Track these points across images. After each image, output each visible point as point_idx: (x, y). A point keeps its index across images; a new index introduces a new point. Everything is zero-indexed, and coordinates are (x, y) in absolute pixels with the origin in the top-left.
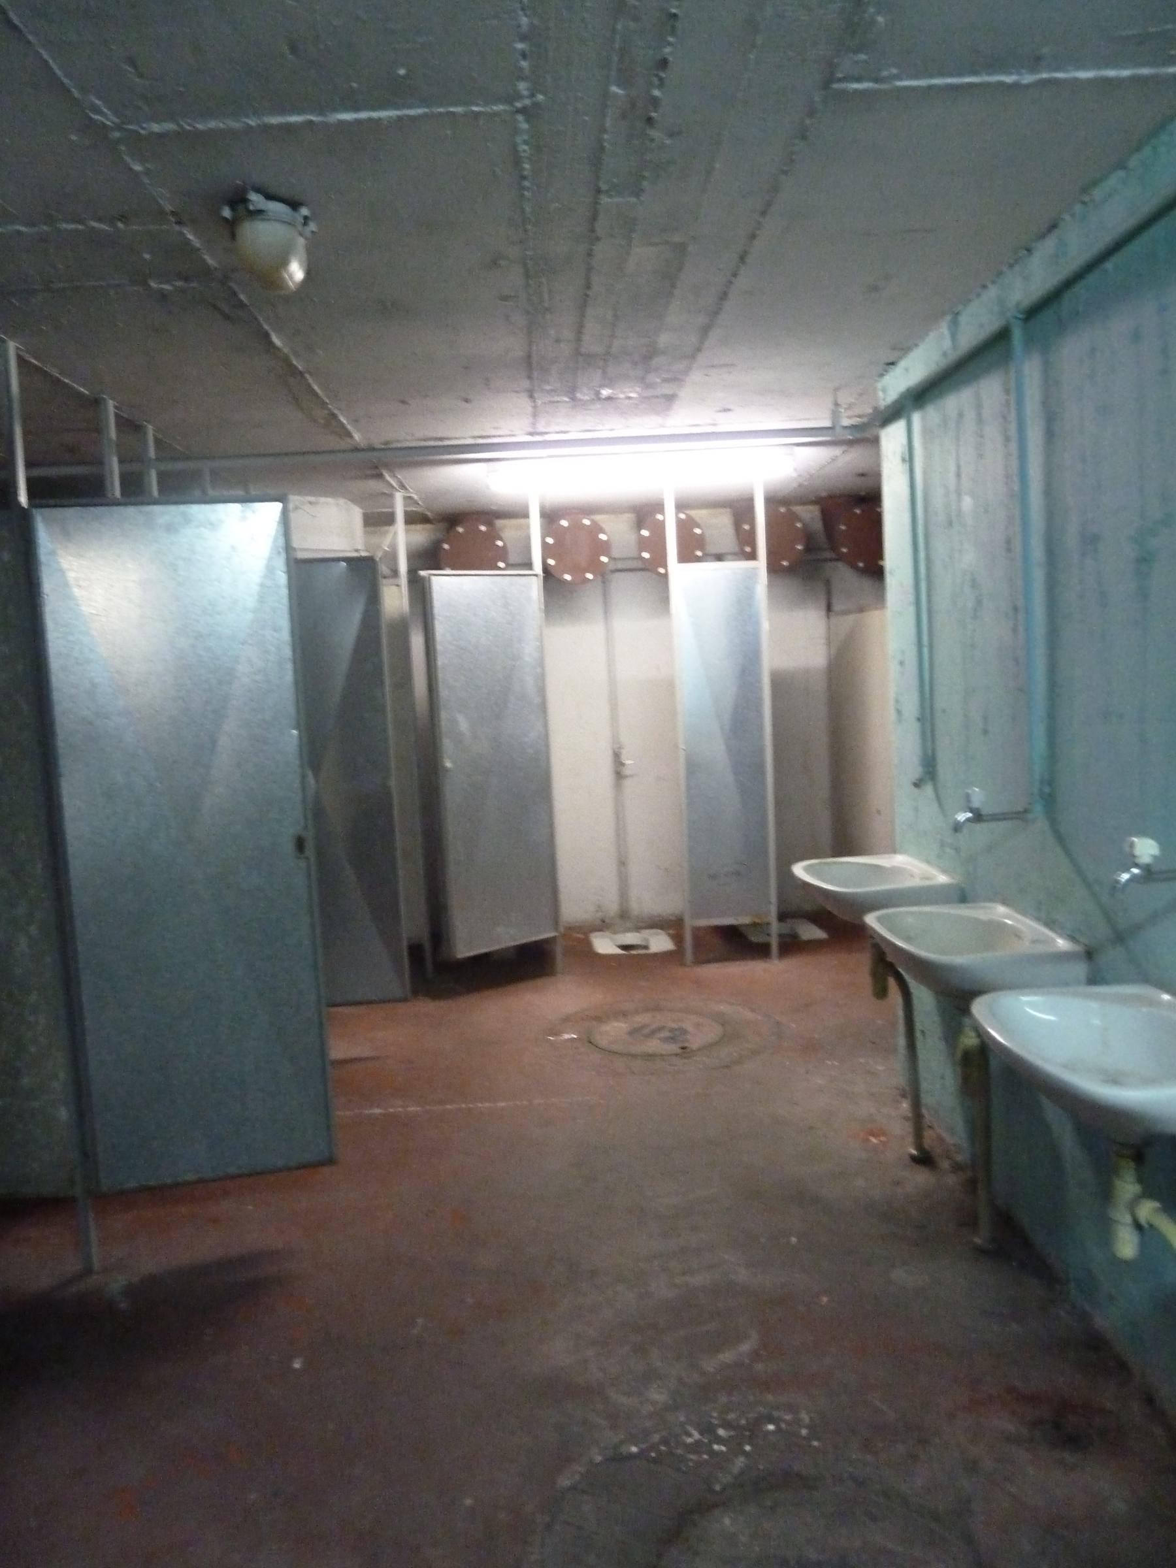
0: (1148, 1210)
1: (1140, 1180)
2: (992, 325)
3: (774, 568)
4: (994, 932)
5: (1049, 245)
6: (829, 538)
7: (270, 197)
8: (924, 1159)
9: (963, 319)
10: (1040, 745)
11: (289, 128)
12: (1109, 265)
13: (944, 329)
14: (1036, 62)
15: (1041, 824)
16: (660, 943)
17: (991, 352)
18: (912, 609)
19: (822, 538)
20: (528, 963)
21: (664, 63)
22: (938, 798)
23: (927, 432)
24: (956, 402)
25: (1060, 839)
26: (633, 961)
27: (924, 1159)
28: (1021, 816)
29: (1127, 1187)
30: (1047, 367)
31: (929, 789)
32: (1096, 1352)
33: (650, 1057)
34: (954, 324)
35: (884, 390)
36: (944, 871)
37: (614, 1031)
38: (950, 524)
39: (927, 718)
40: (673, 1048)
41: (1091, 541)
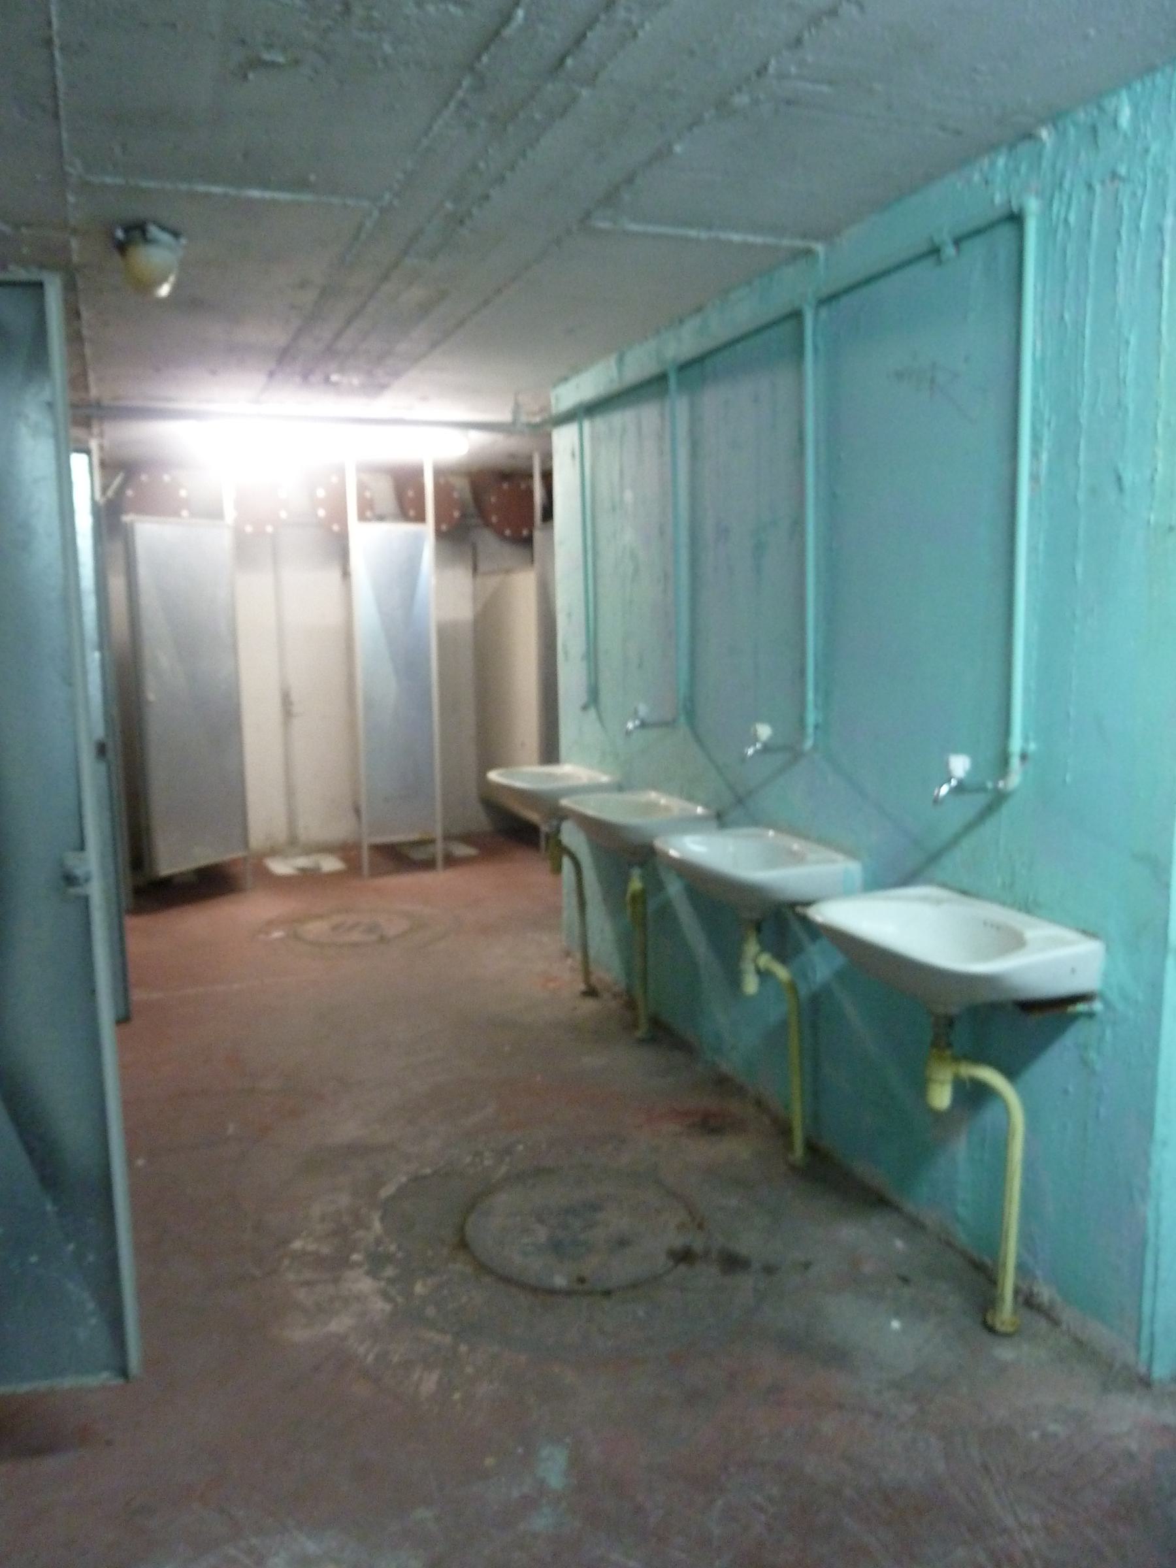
0: (765, 960)
1: (760, 942)
2: (651, 368)
3: (440, 535)
4: (652, 807)
5: (693, 323)
6: (496, 508)
7: (163, 228)
8: (591, 992)
9: (629, 358)
10: (684, 675)
11: (207, 195)
12: (739, 347)
13: (612, 360)
14: (710, 227)
15: (683, 729)
16: (331, 864)
17: (651, 387)
18: (581, 571)
19: (472, 509)
20: (212, 883)
21: (487, 197)
22: (600, 718)
23: (595, 438)
24: (622, 419)
25: (698, 740)
26: (309, 879)
27: (591, 992)
28: (668, 724)
29: (752, 947)
30: (692, 406)
31: (592, 713)
32: (723, 1083)
33: (355, 945)
34: (621, 360)
35: (557, 399)
36: (605, 772)
37: (315, 929)
38: (614, 509)
39: (592, 655)
40: (374, 937)
41: (723, 532)
